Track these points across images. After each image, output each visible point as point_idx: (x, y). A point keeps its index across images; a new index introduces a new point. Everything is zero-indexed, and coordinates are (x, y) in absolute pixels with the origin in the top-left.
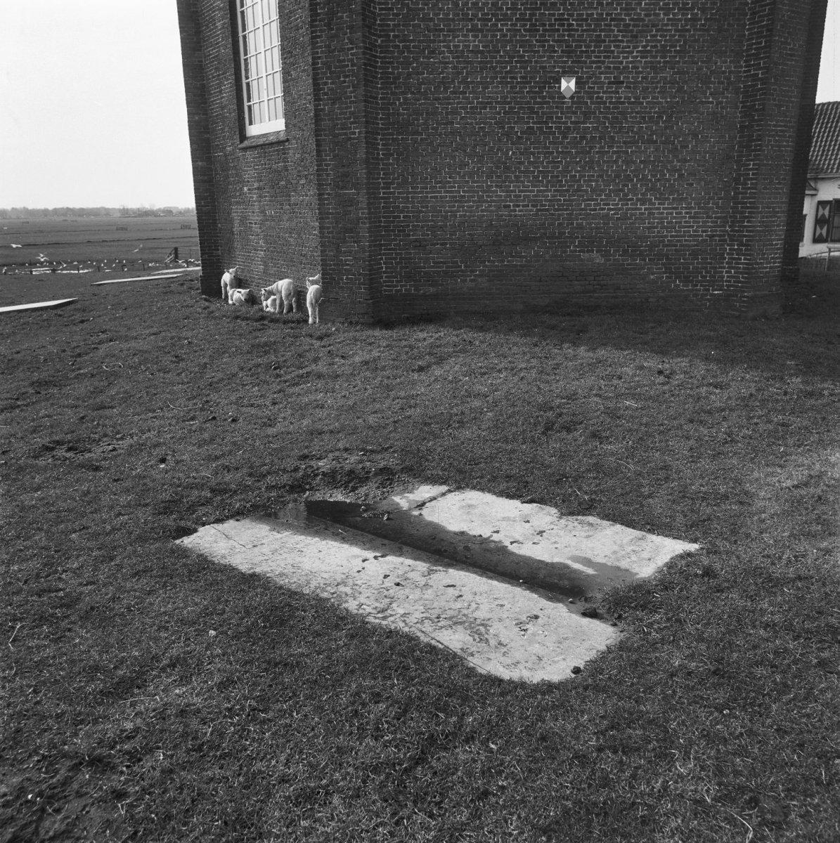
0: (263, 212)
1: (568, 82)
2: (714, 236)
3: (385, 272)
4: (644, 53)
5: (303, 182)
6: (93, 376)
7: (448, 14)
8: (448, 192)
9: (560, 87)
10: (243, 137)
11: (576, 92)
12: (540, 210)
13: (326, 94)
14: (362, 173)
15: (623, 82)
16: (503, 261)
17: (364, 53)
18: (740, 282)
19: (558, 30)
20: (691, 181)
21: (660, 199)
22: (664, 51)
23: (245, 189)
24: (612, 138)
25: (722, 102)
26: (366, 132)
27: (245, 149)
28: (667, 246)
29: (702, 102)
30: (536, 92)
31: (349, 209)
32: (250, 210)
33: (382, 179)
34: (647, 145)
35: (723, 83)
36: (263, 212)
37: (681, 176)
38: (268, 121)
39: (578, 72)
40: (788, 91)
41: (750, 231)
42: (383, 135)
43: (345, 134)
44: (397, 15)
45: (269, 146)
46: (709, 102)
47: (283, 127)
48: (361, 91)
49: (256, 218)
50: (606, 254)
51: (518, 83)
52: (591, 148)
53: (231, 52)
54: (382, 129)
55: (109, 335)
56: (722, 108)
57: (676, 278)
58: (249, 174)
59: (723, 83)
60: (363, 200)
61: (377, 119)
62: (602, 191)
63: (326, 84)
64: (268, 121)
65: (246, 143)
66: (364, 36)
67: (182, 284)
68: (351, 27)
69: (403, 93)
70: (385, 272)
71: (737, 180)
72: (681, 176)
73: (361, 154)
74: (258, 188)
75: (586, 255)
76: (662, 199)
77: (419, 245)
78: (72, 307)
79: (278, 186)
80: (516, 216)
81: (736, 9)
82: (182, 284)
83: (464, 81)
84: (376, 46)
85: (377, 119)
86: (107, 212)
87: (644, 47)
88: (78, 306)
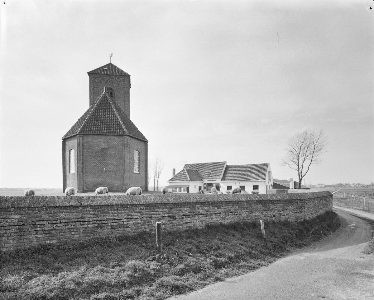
10: (70, 173)
38: (136, 154)
58: (70, 177)
60: (82, 180)
77: (89, 185)
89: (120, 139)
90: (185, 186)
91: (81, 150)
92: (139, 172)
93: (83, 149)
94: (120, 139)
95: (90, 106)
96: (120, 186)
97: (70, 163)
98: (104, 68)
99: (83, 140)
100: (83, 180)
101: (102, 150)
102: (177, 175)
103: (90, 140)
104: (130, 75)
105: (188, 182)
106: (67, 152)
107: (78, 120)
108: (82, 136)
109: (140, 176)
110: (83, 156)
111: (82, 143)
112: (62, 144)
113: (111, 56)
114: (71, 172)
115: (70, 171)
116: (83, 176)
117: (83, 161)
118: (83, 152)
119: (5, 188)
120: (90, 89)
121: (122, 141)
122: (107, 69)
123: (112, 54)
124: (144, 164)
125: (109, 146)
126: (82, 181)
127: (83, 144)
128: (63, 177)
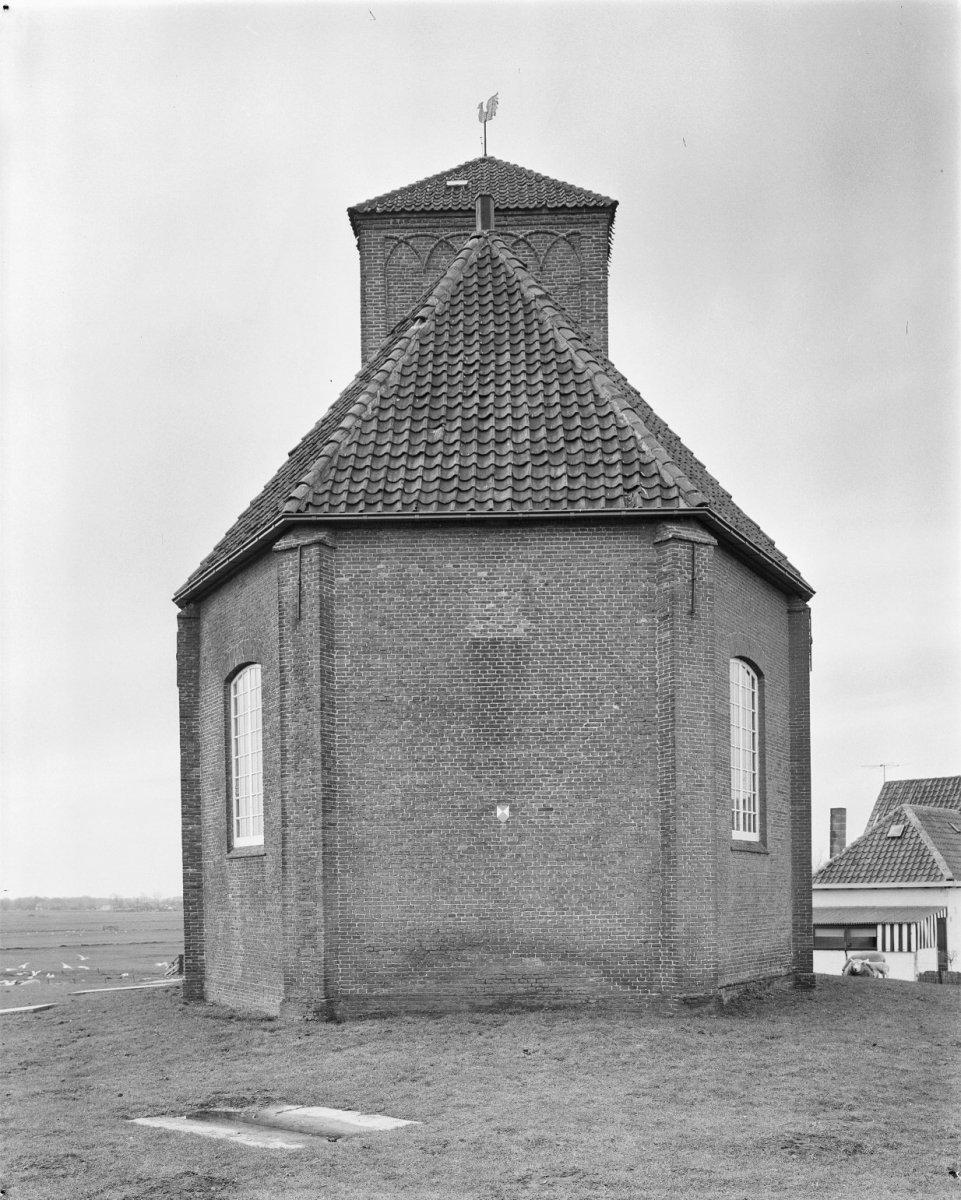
0: (243, 918)
1: (503, 809)
2: (647, 942)
3: (341, 975)
4: (570, 784)
5: (276, 892)
6: (71, 1059)
7: (397, 757)
8: (398, 903)
9: (496, 814)
10: (230, 848)
11: (510, 818)
12: (482, 919)
13: (291, 821)
14: (319, 886)
15: (552, 809)
16: (449, 964)
17: (322, 790)
18: (673, 984)
19: (492, 768)
20: (621, 892)
21: (593, 908)
22: (587, 782)
23: (230, 896)
24: (546, 856)
25: (643, 825)
26: (324, 853)
27: (231, 859)
28: (604, 951)
29: (625, 825)
30: (475, 818)
31: (309, 918)
32: (233, 921)
33: (340, 892)
34: (578, 862)
35: (642, 809)
36: (243, 918)
37: (611, 888)
38: (250, 836)
39: (511, 801)
40: (701, 815)
41: (676, 937)
42: (341, 854)
43: (306, 855)
44: (354, 758)
45: (253, 858)
46: (632, 825)
47: (262, 842)
48: (320, 819)
49: (238, 924)
50: (546, 959)
51: (459, 811)
52: (526, 865)
53: (224, 772)
54: (339, 850)
55: (88, 1032)
56: (644, 829)
57: (614, 980)
58: (234, 882)
59: (642, 809)
60: (320, 909)
61: (335, 841)
62: (539, 902)
63: (292, 813)
64: (250, 836)
65: (233, 854)
66: (323, 776)
67: (167, 991)
68: (313, 770)
69: (358, 820)
70: (341, 975)
71: (663, 891)
72: (611, 888)
73: (319, 871)
74: (241, 896)
75: (528, 959)
76: (596, 910)
77: (373, 950)
78: (51, 1011)
79: (257, 897)
80: (460, 924)
81: (648, 749)
82: (167, 991)
83: (411, 810)
84: (335, 783)
85: (335, 841)
86: (92, 904)
87: (570, 780)
88: (58, 1009)
89: (629, 558)
90: (925, 910)
91: (314, 664)
92: (754, 837)
93: (328, 647)
94: (629, 558)
95: (364, 361)
96: (631, 959)
97: (228, 773)
98: (449, 183)
99: (326, 575)
100: (328, 904)
101: (485, 652)
102: (855, 846)
103: (383, 571)
104: (614, 197)
105: (941, 888)
106: (211, 691)
107: (290, 454)
108: (319, 543)
109: (762, 867)
110: (327, 705)
111: (315, 600)
112: (179, 634)
113: (487, 114)
114: (239, 842)
115: (229, 831)
116: (329, 878)
117: (327, 752)
118: (326, 676)
119: (36, 898)
120: (363, 313)
121: (651, 567)
122: (465, 182)
123: (494, 101)
124: (788, 775)
125: (535, 620)
126: (318, 919)
127: (326, 606)
128: (186, 877)
